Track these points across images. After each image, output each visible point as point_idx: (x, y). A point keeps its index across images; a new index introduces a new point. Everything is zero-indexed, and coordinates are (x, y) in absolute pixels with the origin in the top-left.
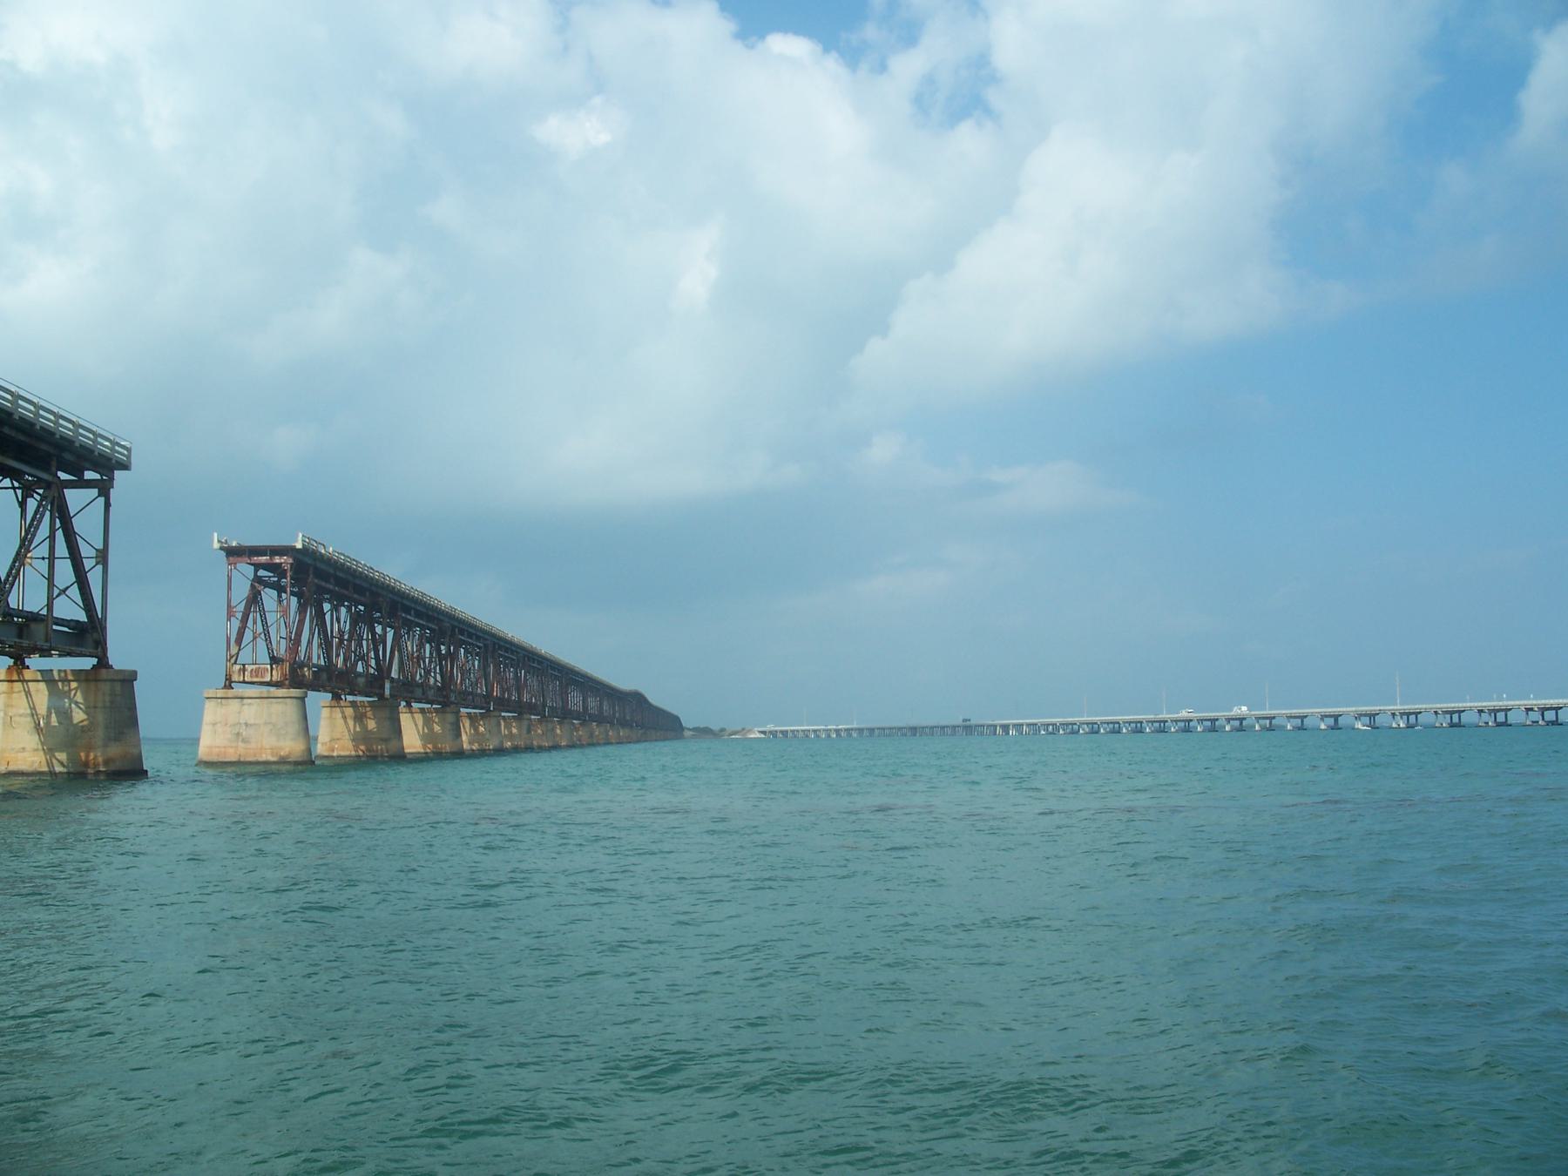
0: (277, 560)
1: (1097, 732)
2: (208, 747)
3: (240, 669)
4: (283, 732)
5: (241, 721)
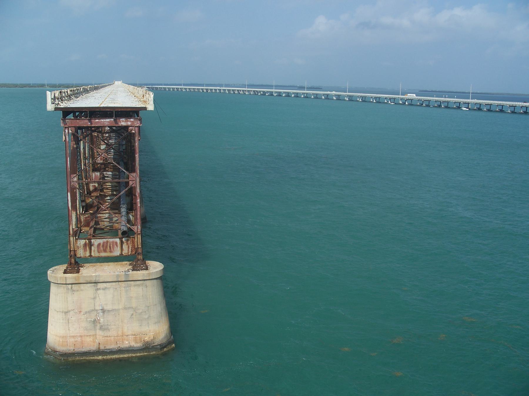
0: (123, 122)
1: (265, 95)
2: (63, 337)
3: (85, 245)
4: (146, 317)
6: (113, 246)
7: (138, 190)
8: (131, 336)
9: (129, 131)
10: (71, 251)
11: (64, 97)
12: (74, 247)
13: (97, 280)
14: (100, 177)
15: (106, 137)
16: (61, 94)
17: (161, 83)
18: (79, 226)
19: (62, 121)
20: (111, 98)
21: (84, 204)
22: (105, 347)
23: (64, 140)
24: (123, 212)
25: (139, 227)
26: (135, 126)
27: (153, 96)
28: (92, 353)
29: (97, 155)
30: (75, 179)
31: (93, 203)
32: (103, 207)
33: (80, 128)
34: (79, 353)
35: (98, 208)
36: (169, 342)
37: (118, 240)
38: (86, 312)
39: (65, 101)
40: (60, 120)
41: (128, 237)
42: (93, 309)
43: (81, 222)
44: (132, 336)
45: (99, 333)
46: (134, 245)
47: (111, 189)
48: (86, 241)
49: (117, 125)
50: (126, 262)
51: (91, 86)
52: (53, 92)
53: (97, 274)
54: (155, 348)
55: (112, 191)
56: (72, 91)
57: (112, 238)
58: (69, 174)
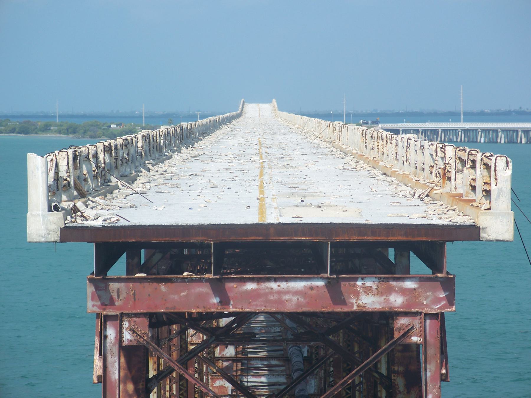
9: (397, 335)
15: (227, 359)
16: (75, 167)
17: (452, 109)
19: (90, 289)
23: (99, 377)
26: (426, 315)
27: (509, 172)
39: (97, 199)
52: (52, 157)
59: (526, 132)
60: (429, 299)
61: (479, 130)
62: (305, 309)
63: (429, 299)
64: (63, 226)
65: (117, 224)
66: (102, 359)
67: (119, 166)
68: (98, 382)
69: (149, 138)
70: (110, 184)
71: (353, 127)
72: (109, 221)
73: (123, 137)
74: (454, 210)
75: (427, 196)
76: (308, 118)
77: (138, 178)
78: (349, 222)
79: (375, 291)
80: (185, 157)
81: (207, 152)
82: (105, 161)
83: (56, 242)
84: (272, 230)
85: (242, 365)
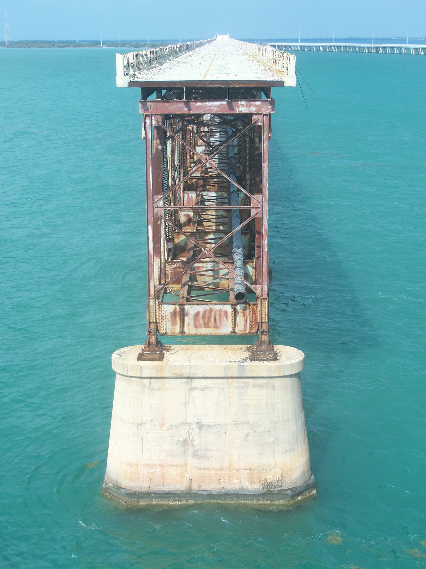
3: (174, 314)
4: (271, 440)
5: (189, 420)
6: (220, 317)
7: (265, 224)
8: (243, 471)
9: (253, 122)
10: (150, 323)
11: (142, 64)
12: (156, 317)
13: (193, 373)
14: (197, 201)
15: (205, 132)
16: (137, 59)
17: (296, 38)
18: (163, 282)
19: (140, 105)
20: (218, 65)
21: (171, 245)
22: (200, 486)
23: (144, 137)
24: (238, 261)
25: (266, 287)
26: (264, 114)
27: (295, 60)
28: (178, 494)
29: (191, 163)
30: (161, 203)
31: (185, 244)
32: (206, 252)
33: (167, 117)
34: (158, 494)
35: (195, 255)
36: (307, 485)
37: (228, 308)
38: (173, 425)
39: (145, 71)
40: (138, 103)
41: (245, 303)
42: (184, 421)
43: (166, 275)
44: (247, 471)
45: (192, 462)
46: (256, 317)
47: (214, 220)
48: (176, 307)
49: (231, 112)
50: (241, 346)
51: (182, 45)
52: (126, 55)
53: (193, 363)
54: (284, 494)
55: (218, 224)
56: (152, 52)
57: (220, 304)
58: (150, 195)
59: (423, 49)
60: (265, 109)
61: (306, 46)
62: (219, 113)
63: (265, 109)
64: (130, 81)
65: (149, 81)
66: (145, 131)
67: (157, 59)
68: (144, 139)
69: (172, 48)
70: (152, 65)
71: (250, 44)
72: (146, 79)
73: (160, 48)
74: (276, 75)
75: (269, 70)
76: (238, 41)
77: (165, 63)
78: (235, 80)
79: (245, 106)
80: (187, 56)
81: (196, 54)
82: (151, 57)
83: (127, 87)
84: (207, 83)
85: (210, 134)
